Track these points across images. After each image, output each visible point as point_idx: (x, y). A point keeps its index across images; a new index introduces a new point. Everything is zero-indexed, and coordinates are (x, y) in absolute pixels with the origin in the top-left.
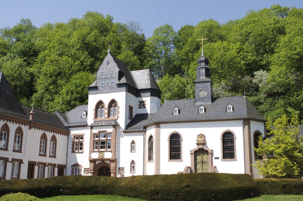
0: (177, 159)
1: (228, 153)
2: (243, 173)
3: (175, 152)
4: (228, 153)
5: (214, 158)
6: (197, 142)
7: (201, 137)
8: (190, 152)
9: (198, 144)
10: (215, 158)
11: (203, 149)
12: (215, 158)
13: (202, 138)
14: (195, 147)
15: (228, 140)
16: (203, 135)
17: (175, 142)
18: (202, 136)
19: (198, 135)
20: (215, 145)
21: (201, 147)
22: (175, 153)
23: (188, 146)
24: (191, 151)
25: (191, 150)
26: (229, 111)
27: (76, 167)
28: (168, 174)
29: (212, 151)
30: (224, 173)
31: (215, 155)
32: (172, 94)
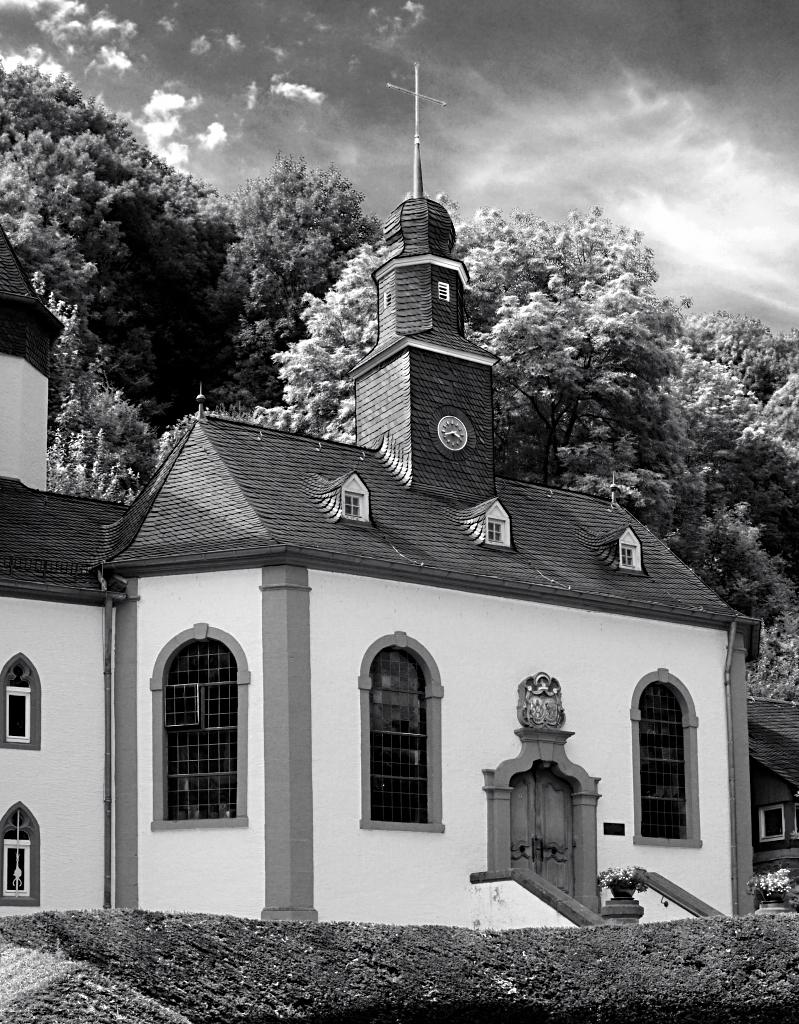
1: (665, 814)
4: (665, 814)
7: (544, 694)
8: (482, 781)
10: (606, 825)
12: (606, 825)
13: (548, 701)
14: (507, 748)
18: (550, 690)
19: (530, 681)
21: (547, 754)
22: (400, 790)
23: (473, 741)
24: (488, 773)
29: (597, 781)
31: (607, 813)
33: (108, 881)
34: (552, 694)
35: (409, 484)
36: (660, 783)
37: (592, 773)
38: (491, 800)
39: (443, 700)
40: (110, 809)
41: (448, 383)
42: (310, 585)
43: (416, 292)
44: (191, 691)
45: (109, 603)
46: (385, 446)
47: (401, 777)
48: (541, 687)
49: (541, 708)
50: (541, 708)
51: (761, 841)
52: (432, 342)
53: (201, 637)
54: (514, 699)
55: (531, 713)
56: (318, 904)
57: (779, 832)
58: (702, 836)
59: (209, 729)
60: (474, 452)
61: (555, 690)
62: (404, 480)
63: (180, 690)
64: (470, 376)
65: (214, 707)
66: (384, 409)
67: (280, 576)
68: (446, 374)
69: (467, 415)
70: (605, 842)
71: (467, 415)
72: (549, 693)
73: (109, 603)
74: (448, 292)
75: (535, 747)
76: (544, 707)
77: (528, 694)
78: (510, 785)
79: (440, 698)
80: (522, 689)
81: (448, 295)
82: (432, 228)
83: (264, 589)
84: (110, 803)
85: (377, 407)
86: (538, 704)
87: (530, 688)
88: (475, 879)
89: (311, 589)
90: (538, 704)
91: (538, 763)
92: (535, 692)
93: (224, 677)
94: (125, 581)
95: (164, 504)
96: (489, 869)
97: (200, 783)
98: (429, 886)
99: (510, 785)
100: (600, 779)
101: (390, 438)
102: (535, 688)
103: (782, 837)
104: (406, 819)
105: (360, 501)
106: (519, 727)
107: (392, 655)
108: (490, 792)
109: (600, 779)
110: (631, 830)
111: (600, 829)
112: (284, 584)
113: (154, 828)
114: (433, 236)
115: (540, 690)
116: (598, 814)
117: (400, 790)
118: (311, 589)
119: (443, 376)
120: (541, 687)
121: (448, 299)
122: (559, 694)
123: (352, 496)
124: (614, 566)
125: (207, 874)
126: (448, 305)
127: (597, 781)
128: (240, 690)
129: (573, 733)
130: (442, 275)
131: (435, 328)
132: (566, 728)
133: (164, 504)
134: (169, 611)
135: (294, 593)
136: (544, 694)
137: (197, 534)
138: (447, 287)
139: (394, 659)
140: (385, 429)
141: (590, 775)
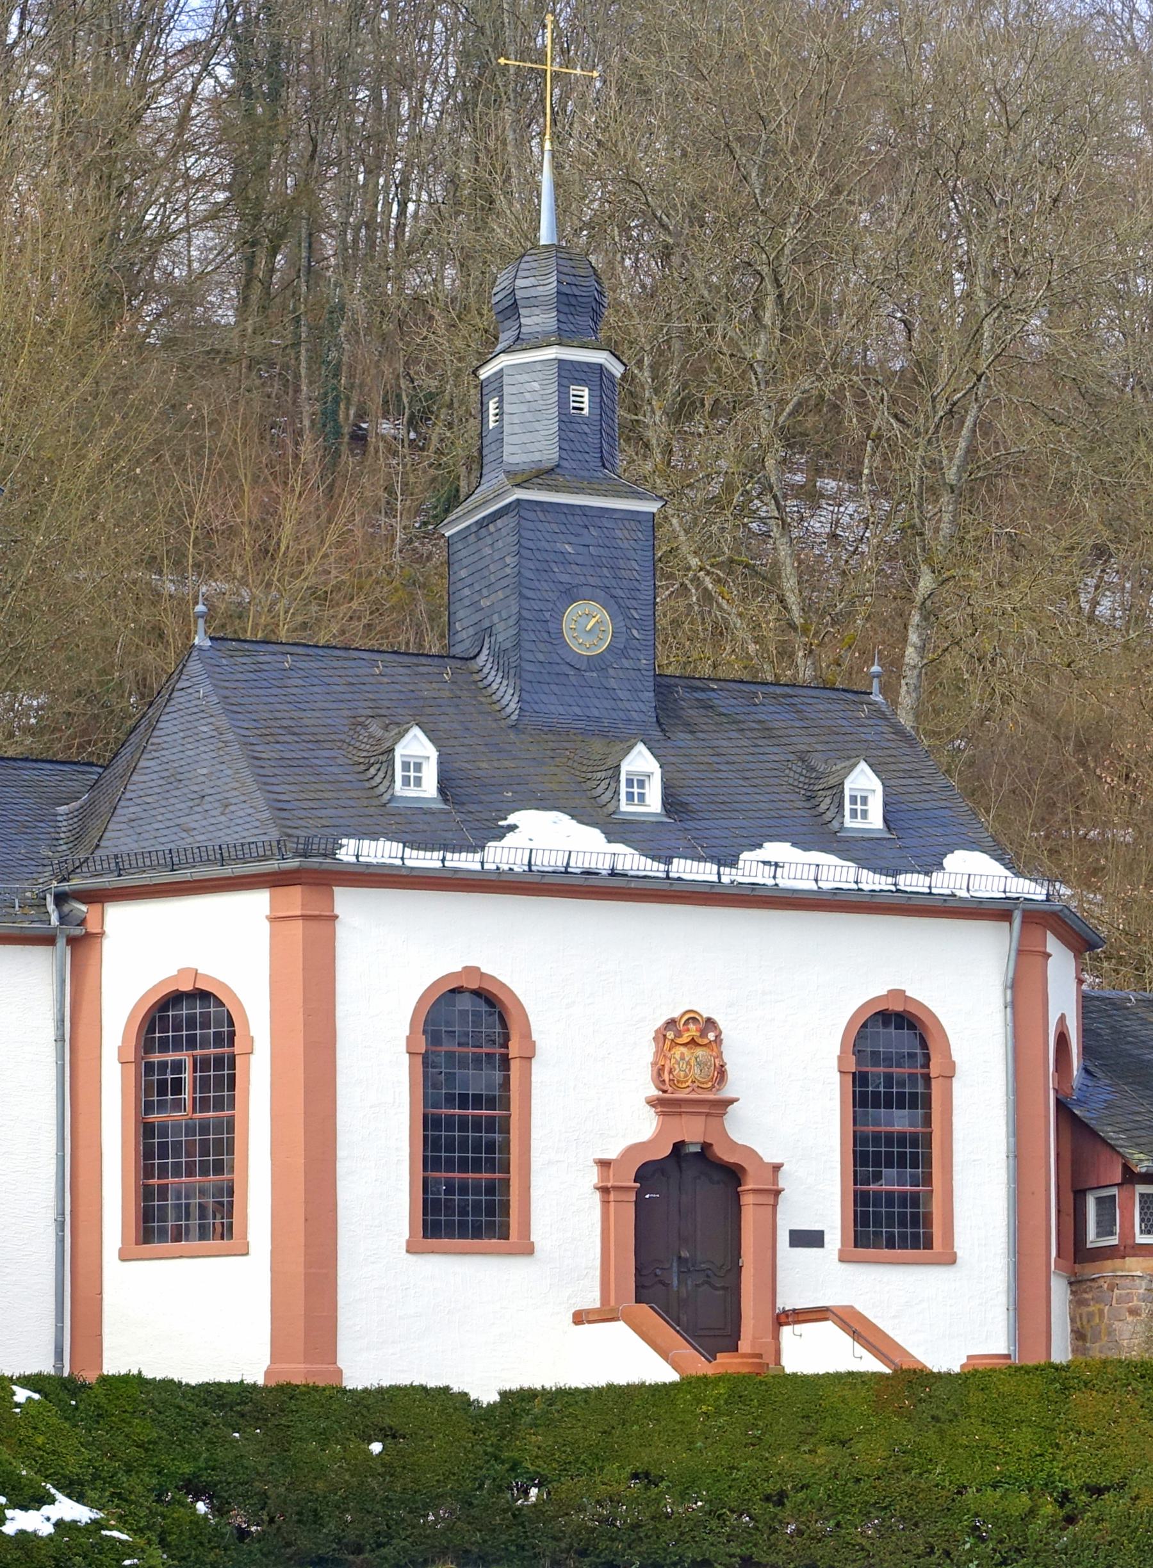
0: (477, 1233)
1: (894, 1209)
2: (256, 1375)
3: (463, 1166)
4: (894, 1209)
5: (783, 1238)
6: (654, 1092)
7: (693, 1042)
8: (593, 1176)
9: (666, 1105)
10: (793, 1233)
11: (706, 1146)
12: (793, 1233)
13: (700, 1052)
14: (635, 1127)
15: (892, 1066)
16: (710, 1023)
17: (471, 1053)
18: (703, 1033)
19: (671, 1023)
20: (795, 1127)
21: (692, 1131)
22: (467, 1186)
23: (583, 1118)
24: (604, 1164)
25: (612, 1154)
26: (411, 792)
27: (607, 1308)
28: (623, 1382)
29: (777, 1168)
30: (169, 1386)
31: (790, 1218)
32: (447, 398)
33: (60, 1331)
34: (705, 1041)
35: (514, 717)
36: (889, 1165)
37: (769, 1156)
38: (605, 1203)
39: (533, 1061)
40: (63, 1231)
41: (581, 549)
42: (337, 911)
43: (534, 405)
44: (178, 1067)
45: (61, 942)
46: (485, 652)
47: (471, 1175)
48: (691, 1037)
49: (688, 1063)
50: (688, 1063)
51: (1089, 1246)
52: (556, 489)
53: (186, 987)
54: (647, 1052)
55: (671, 1072)
56: (344, 1360)
57: (1112, 1233)
58: (956, 1244)
59: (198, 1115)
60: (624, 653)
61: (711, 1036)
62: (509, 710)
63: (163, 1065)
64: (618, 533)
65: (204, 1084)
66: (485, 592)
67: (295, 898)
68: (577, 535)
69: (613, 597)
70: (790, 1258)
71: (613, 597)
72: (700, 1041)
73: (61, 942)
74: (586, 399)
75: (675, 1120)
76: (693, 1062)
77: (668, 1043)
78: (635, 1181)
79: (530, 1058)
80: (660, 1037)
81: (586, 406)
82: (564, 299)
83: (273, 919)
84: (63, 1222)
85: (477, 587)
86: (682, 1058)
87: (670, 1035)
88: (580, 1318)
89: (337, 917)
90: (682, 1058)
91: (678, 1147)
92: (679, 1041)
93: (219, 1040)
94: (84, 908)
95: (142, 786)
96: (602, 1304)
97: (181, 1189)
98: (528, 1323)
99: (635, 1181)
100: (782, 1165)
101: (493, 639)
102: (679, 1034)
103: (1114, 1241)
104: (477, 1234)
105: (424, 767)
106: (654, 1092)
107: (458, 997)
108: (604, 1190)
109: (782, 1165)
110: (834, 1239)
111: (783, 1238)
112: (298, 913)
113: (124, 1257)
114: (566, 309)
115: (685, 1038)
116: (779, 1216)
117: (467, 1186)
118: (337, 917)
119: (573, 539)
120: (691, 1037)
121: (586, 412)
122: (718, 1040)
123: (412, 761)
124: (835, 825)
125: (188, 1320)
126: (586, 421)
127: (777, 1168)
128: (239, 1061)
129: (737, 1100)
130: (577, 375)
131: (564, 464)
132: (727, 1092)
133: (142, 786)
134: (147, 946)
135: (310, 923)
136: (693, 1042)
137: (184, 835)
138: (586, 392)
139: (465, 1003)
140: (486, 624)
141: (767, 1159)
